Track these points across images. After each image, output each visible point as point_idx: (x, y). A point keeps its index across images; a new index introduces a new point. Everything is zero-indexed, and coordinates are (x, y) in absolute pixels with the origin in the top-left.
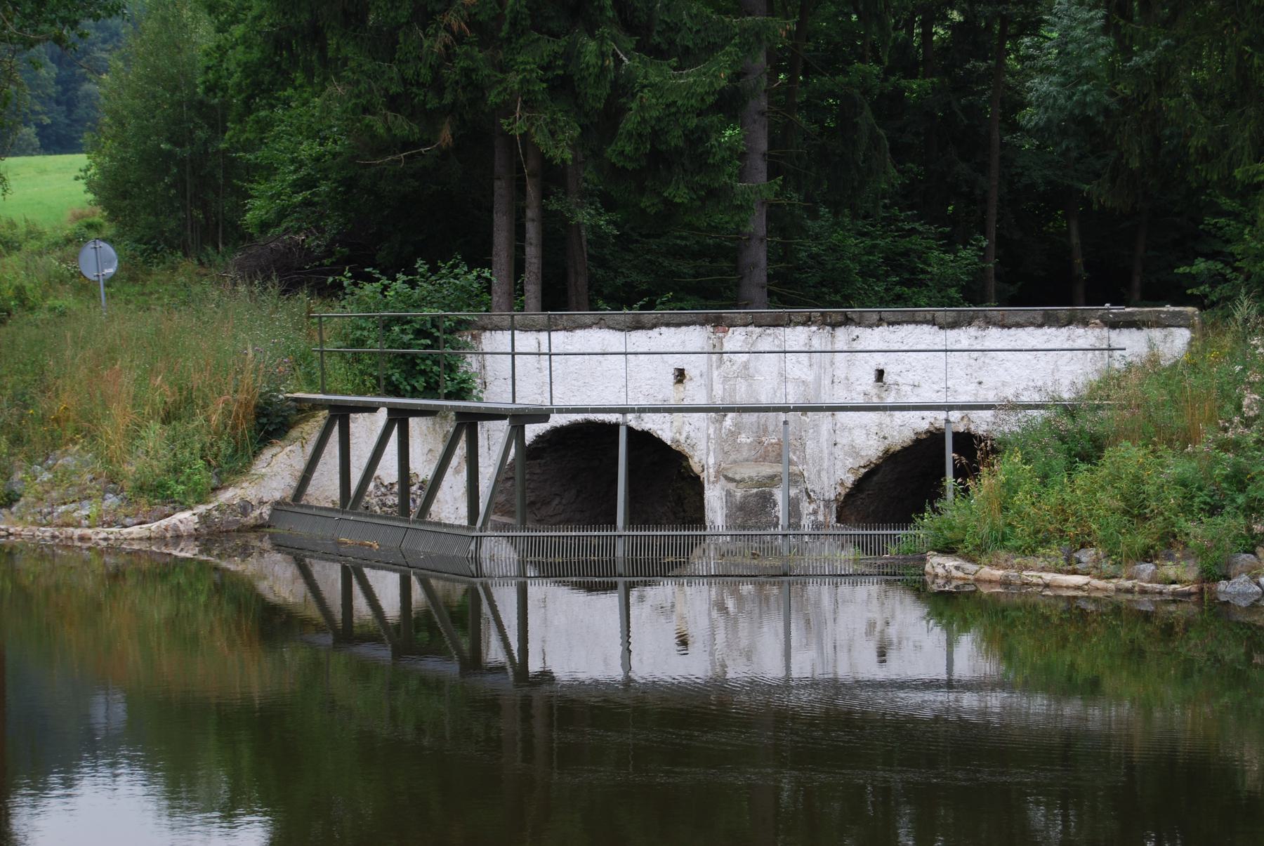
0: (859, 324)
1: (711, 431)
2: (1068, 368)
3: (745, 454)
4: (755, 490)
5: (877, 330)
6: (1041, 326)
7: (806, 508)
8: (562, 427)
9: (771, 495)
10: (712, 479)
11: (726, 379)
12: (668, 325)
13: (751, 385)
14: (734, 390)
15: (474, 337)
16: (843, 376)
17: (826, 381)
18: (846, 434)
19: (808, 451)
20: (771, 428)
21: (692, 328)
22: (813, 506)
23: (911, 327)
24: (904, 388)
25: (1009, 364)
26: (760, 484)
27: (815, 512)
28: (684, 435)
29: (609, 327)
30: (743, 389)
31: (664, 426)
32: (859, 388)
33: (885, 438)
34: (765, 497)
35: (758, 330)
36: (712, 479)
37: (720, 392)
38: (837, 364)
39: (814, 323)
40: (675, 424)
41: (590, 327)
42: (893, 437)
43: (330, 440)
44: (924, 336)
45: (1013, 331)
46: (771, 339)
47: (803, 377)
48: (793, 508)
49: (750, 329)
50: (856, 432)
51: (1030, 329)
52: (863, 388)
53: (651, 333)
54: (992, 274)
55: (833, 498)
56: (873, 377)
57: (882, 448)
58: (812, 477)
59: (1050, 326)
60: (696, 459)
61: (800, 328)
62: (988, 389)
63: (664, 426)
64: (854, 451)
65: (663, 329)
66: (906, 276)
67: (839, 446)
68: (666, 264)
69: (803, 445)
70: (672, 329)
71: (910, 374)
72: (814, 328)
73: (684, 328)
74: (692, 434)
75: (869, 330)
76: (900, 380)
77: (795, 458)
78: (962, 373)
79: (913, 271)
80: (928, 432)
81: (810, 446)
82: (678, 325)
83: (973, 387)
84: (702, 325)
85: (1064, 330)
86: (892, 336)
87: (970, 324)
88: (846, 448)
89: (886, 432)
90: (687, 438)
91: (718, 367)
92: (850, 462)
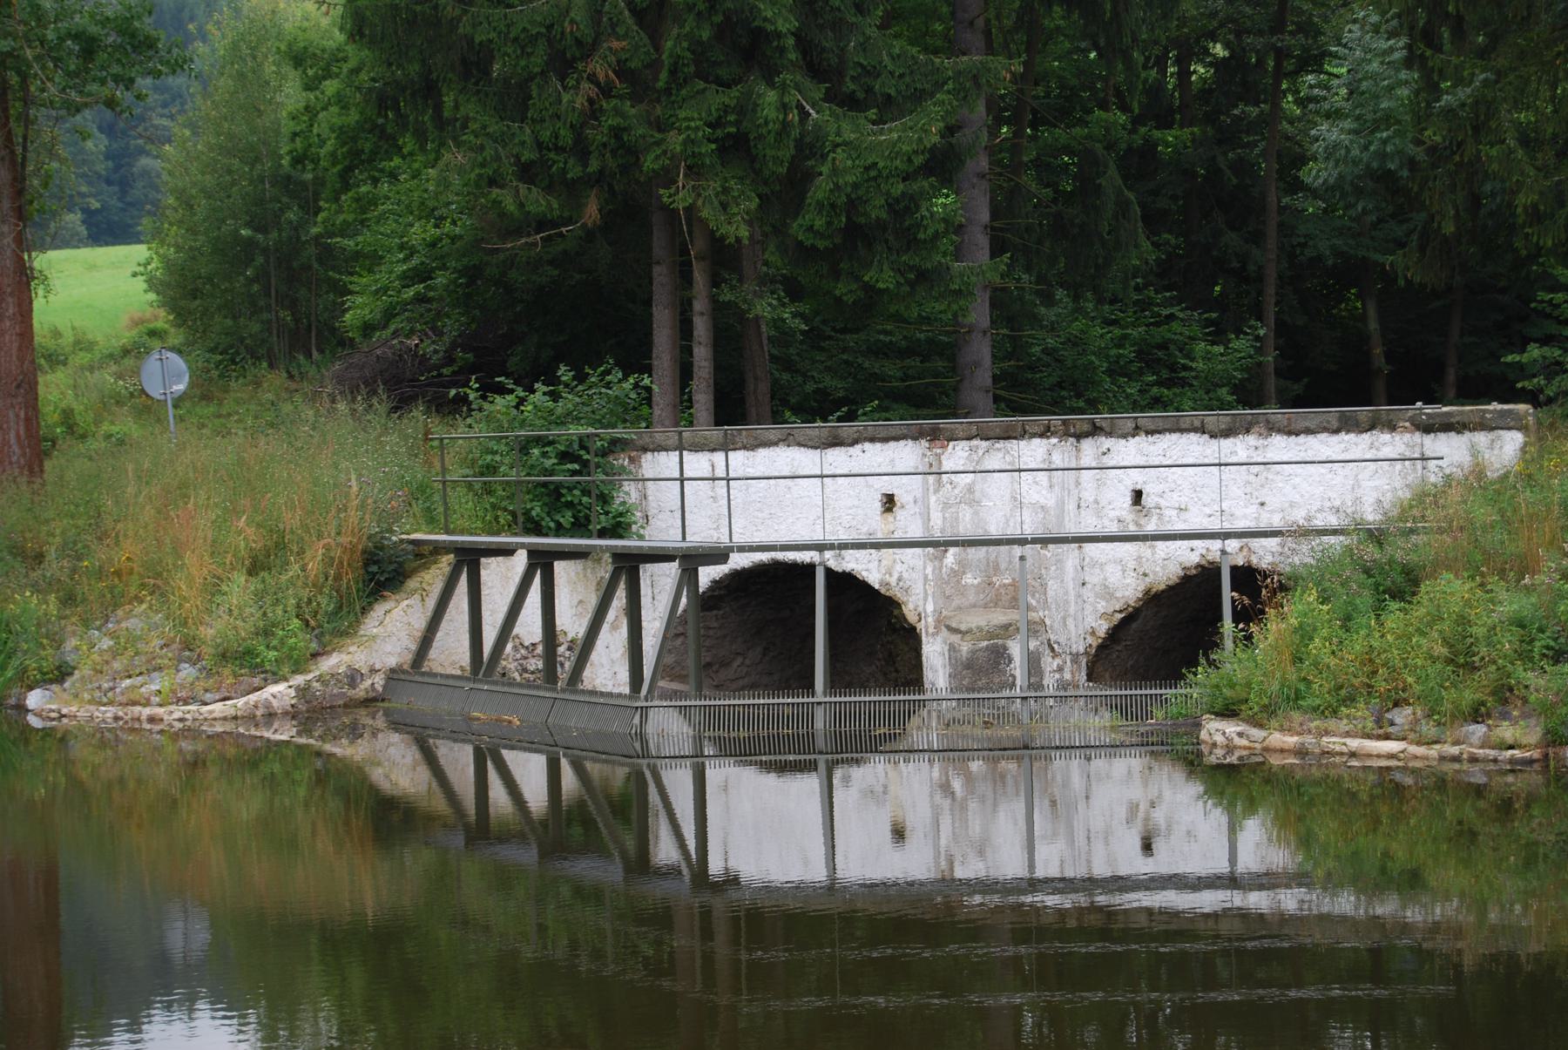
0: (1110, 434)
1: (929, 570)
2: (1371, 484)
3: (972, 598)
5: (1133, 441)
6: (1336, 431)
7: (1049, 663)
8: (744, 569)
9: (1005, 648)
10: (931, 630)
11: (946, 506)
12: (872, 440)
13: (976, 513)
14: (957, 519)
19: (1050, 593)
20: (1003, 566)
21: (902, 443)
22: (1058, 661)
23: (1175, 436)
24: (1167, 512)
25: (1298, 480)
26: (991, 635)
27: (1060, 669)
28: (896, 576)
29: (800, 445)
30: (968, 518)
31: (871, 566)
32: (1112, 514)
33: (1145, 575)
34: (998, 652)
35: (984, 444)
36: (931, 630)
37: (939, 522)
38: (1084, 484)
39: (1054, 434)
40: (884, 562)
41: (776, 444)
42: (1155, 573)
43: (457, 591)
45: (1302, 439)
46: (1000, 455)
47: (1043, 501)
49: (975, 442)
50: (1110, 568)
51: (1323, 436)
52: (1117, 513)
53: (851, 450)
54: (1271, 369)
55: (1082, 650)
57: (1142, 588)
58: (1056, 626)
59: (1348, 432)
60: (911, 606)
61: (1036, 441)
62: (1272, 512)
63: (871, 566)
64: (1107, 593)
65: (867, 445)
66: (1165, 374)
67: (1089, 586)
68: (867, 364)
69: (1044, 586)
70: (878, 445)
71: (1175, 495)
72: (1054, 440)
73: (892, 444)
74: (905, 575)
75: (1123, 441)
76: (1163, 503)
77: (1034, 603)
78: (1240, 493)
79: (1173, 368)
80: (1199, 566)
81: (1053, 586)
82: (885, 440)
83: (1253, 509)
84: (915, 439)
85: (1366, 436)
86: (1152, 448)
87: (1248, 431)
88: (1097, 589)
89: (1146, 568)
90: (899, 579)
91: (936, 491)
92: (1102, 606)
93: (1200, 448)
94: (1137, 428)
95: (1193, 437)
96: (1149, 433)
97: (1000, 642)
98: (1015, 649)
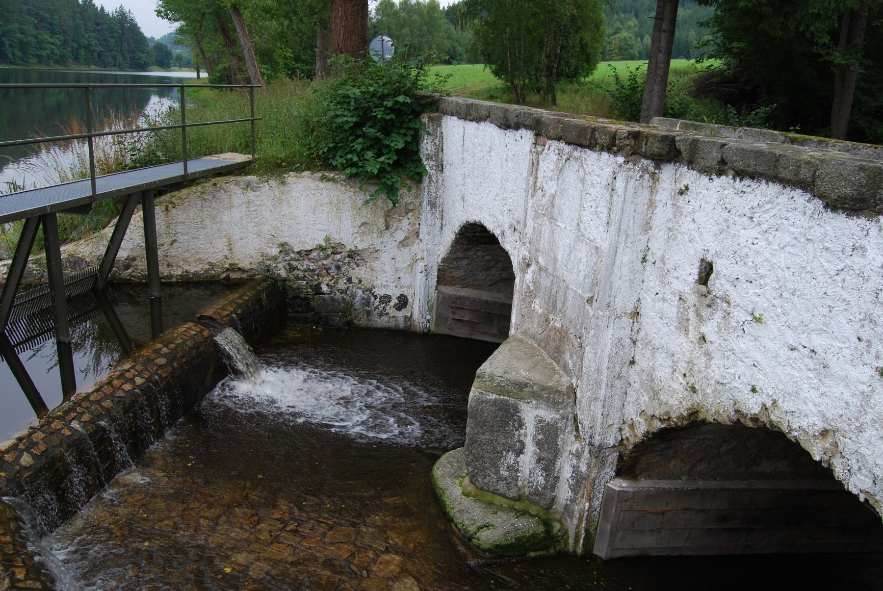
0: (691, 164)
4: (494, 397)
7: (570, 444)
9: (517, 410)
15: (431, 119)
16: (659, 254)
17: (627, 258)
18: (648, 354)
23: (773, 189)
27: (578, 455)
33: (694, 390)
38: (655, 230)
42: (705, 395)
43: (131, 227)
44: (794, 216)
48: (548, 439)
50: (661, 359)
55: (611, 441)
56: (693, 272)
57: (687, 404)
67: (636, 367)
71: (753, 290)
72: (621, 159)
75: (704, 179)
76: (734, 296)
78: (850, 331)
86: (738, 200)
93: (804, 221)
94: (723, 162)
95: (799, 197)
96: (740, 174)
97: (512, 400)
98: (532, 414)
